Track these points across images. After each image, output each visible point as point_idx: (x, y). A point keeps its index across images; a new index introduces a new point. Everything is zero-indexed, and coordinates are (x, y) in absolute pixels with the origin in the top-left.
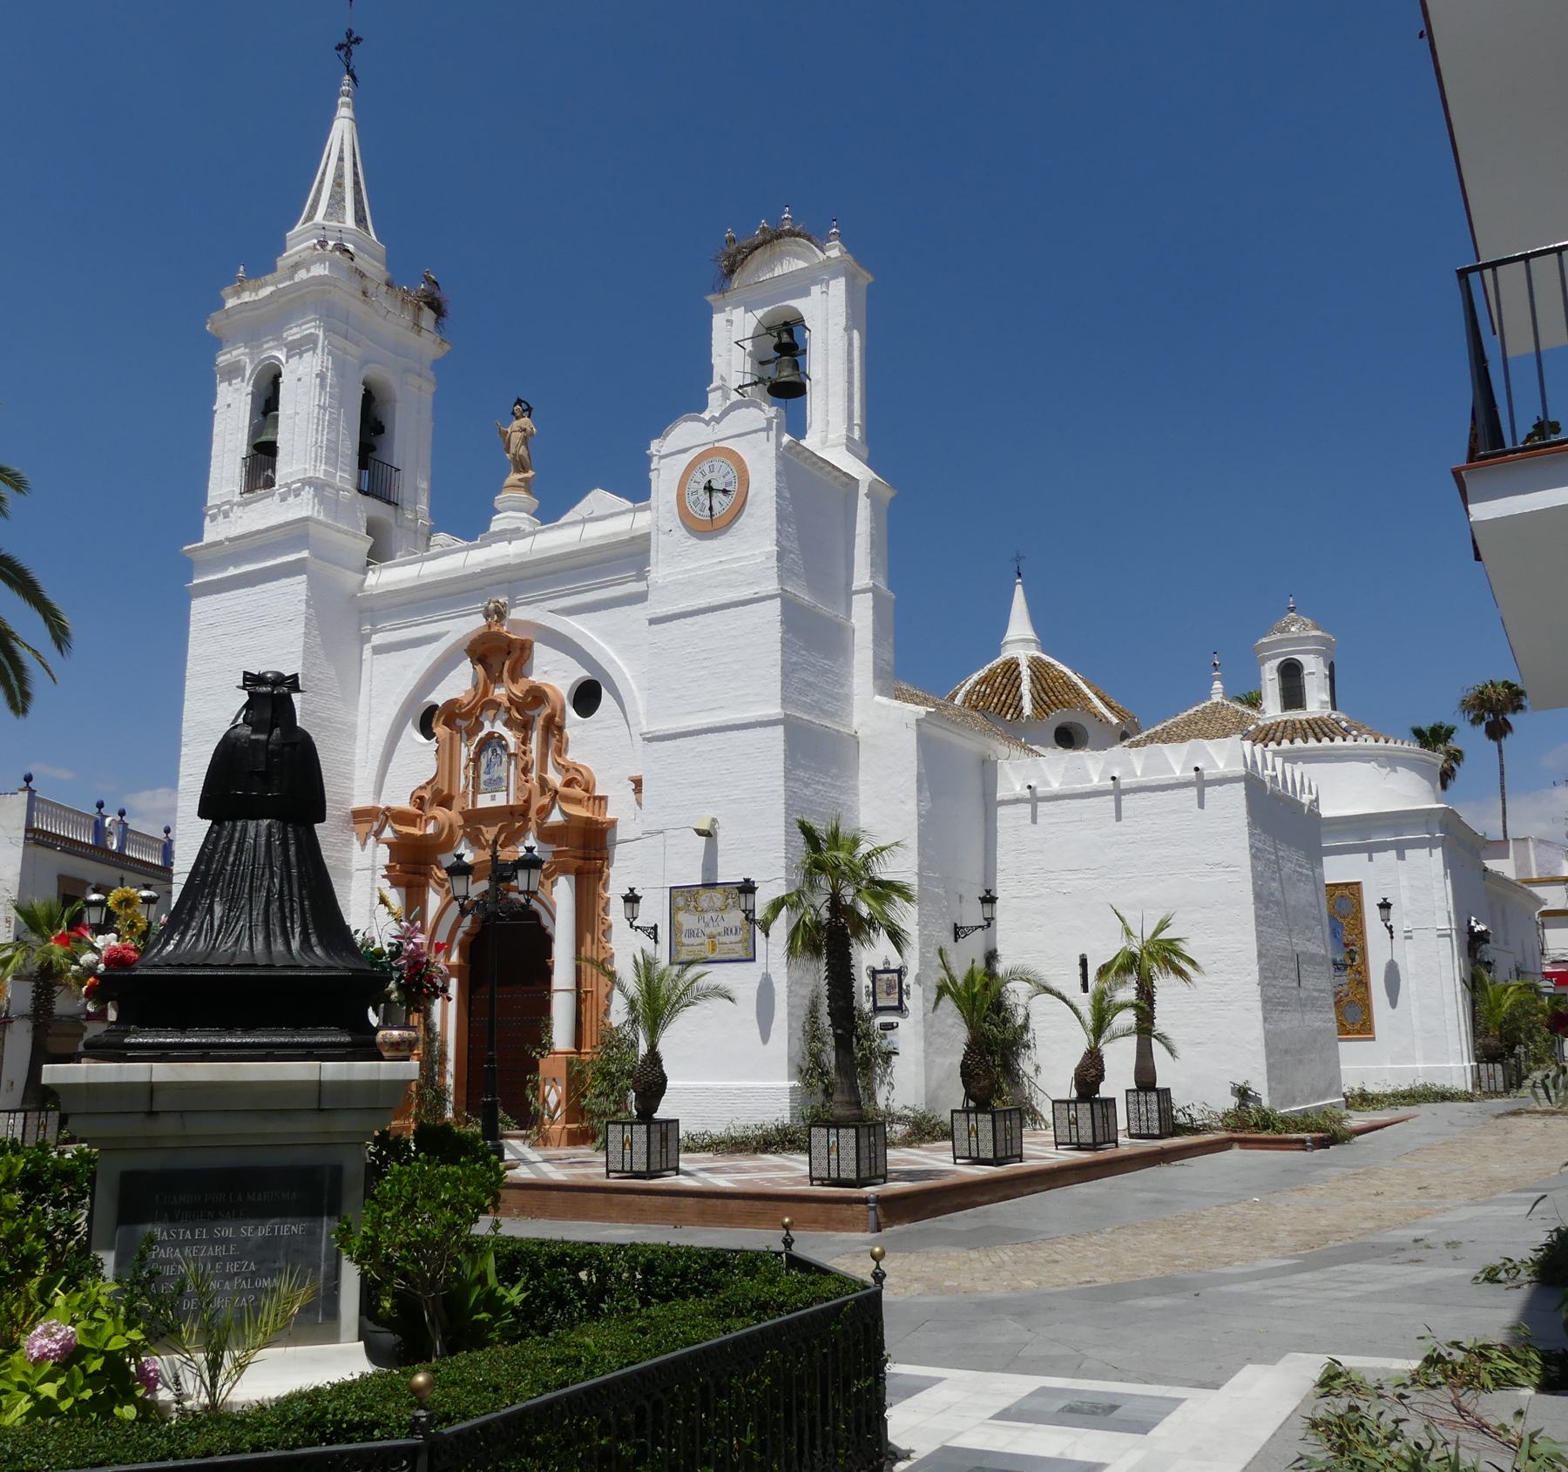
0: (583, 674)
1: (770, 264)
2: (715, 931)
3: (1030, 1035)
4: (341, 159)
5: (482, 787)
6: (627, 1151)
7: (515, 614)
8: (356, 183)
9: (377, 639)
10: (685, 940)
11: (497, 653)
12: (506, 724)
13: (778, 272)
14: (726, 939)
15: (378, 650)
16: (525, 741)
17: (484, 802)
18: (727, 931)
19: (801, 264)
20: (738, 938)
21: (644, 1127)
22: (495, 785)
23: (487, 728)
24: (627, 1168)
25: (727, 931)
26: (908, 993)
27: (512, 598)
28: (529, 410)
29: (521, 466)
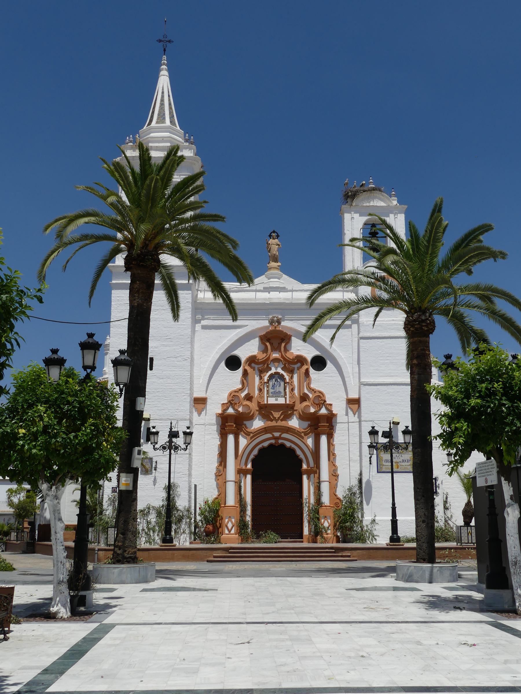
0: (317, 353)
1: (368, 200)
2: (398, 461)
3: (448, 505)
4: (163, 93)
5: (270, 394)
6: (470, 536)
7: (283, 323)
8: (170, 104)
9: (204, 322)
10: (385, 464)
11: (275, 339)
12: (282, 369)
13: (372, 204)
14: (403, 464)
15: (204, 327)
16: (292, 378)
17: (272, 401)
18: (403, 461)
19: (382, 204)
20: (409, 464)
21: (466, 528)
22: (276, 395)
23: (273, 370)
24: (470, 542)
25: (403, 461)
26: (439, 487)
27: (283, 316)
28: (278, 236)
29: (276, 260)
